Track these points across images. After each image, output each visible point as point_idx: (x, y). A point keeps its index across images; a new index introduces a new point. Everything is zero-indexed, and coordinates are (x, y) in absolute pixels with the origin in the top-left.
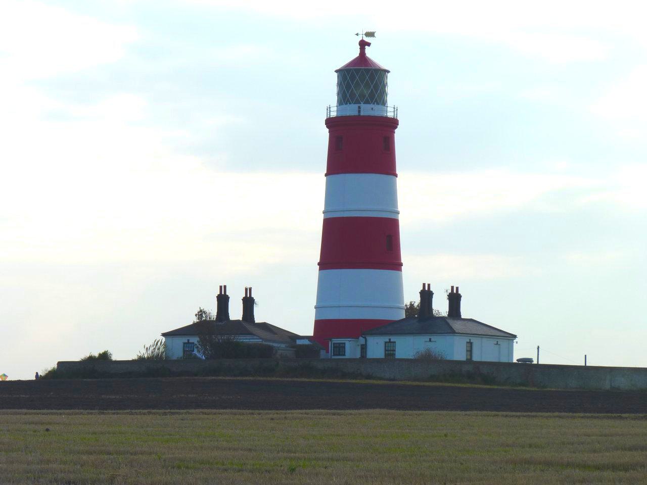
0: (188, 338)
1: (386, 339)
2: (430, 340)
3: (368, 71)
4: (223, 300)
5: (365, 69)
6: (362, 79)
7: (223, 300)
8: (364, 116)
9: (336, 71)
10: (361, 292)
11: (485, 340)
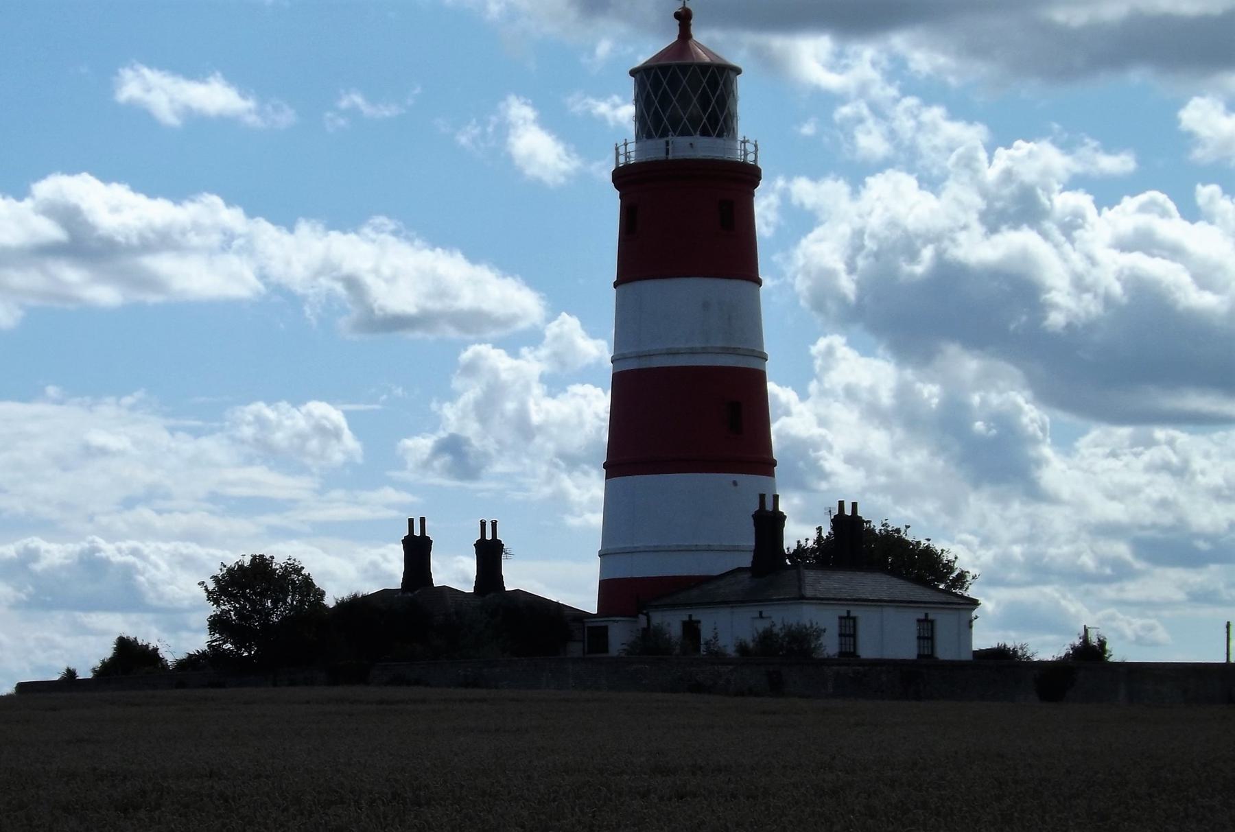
0: (760, 609)
1: (683, 616)
2: (761, 616)
3: (705, 68)
4: (417, 549)
5: (679, 66)
6: (685, 92)
7: (417, 549)
8: (673, 161)
9: (633, 73)
10: (700, 517)
11: (890, 613)
